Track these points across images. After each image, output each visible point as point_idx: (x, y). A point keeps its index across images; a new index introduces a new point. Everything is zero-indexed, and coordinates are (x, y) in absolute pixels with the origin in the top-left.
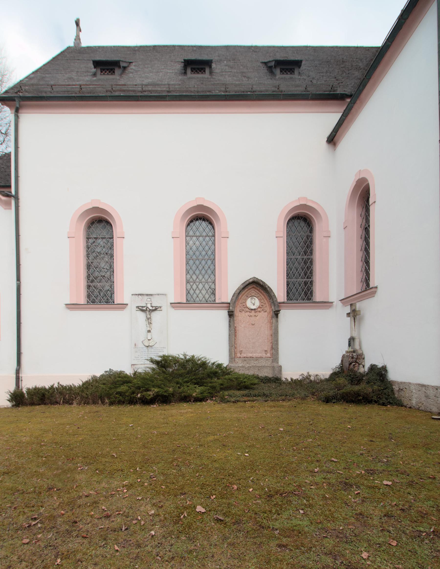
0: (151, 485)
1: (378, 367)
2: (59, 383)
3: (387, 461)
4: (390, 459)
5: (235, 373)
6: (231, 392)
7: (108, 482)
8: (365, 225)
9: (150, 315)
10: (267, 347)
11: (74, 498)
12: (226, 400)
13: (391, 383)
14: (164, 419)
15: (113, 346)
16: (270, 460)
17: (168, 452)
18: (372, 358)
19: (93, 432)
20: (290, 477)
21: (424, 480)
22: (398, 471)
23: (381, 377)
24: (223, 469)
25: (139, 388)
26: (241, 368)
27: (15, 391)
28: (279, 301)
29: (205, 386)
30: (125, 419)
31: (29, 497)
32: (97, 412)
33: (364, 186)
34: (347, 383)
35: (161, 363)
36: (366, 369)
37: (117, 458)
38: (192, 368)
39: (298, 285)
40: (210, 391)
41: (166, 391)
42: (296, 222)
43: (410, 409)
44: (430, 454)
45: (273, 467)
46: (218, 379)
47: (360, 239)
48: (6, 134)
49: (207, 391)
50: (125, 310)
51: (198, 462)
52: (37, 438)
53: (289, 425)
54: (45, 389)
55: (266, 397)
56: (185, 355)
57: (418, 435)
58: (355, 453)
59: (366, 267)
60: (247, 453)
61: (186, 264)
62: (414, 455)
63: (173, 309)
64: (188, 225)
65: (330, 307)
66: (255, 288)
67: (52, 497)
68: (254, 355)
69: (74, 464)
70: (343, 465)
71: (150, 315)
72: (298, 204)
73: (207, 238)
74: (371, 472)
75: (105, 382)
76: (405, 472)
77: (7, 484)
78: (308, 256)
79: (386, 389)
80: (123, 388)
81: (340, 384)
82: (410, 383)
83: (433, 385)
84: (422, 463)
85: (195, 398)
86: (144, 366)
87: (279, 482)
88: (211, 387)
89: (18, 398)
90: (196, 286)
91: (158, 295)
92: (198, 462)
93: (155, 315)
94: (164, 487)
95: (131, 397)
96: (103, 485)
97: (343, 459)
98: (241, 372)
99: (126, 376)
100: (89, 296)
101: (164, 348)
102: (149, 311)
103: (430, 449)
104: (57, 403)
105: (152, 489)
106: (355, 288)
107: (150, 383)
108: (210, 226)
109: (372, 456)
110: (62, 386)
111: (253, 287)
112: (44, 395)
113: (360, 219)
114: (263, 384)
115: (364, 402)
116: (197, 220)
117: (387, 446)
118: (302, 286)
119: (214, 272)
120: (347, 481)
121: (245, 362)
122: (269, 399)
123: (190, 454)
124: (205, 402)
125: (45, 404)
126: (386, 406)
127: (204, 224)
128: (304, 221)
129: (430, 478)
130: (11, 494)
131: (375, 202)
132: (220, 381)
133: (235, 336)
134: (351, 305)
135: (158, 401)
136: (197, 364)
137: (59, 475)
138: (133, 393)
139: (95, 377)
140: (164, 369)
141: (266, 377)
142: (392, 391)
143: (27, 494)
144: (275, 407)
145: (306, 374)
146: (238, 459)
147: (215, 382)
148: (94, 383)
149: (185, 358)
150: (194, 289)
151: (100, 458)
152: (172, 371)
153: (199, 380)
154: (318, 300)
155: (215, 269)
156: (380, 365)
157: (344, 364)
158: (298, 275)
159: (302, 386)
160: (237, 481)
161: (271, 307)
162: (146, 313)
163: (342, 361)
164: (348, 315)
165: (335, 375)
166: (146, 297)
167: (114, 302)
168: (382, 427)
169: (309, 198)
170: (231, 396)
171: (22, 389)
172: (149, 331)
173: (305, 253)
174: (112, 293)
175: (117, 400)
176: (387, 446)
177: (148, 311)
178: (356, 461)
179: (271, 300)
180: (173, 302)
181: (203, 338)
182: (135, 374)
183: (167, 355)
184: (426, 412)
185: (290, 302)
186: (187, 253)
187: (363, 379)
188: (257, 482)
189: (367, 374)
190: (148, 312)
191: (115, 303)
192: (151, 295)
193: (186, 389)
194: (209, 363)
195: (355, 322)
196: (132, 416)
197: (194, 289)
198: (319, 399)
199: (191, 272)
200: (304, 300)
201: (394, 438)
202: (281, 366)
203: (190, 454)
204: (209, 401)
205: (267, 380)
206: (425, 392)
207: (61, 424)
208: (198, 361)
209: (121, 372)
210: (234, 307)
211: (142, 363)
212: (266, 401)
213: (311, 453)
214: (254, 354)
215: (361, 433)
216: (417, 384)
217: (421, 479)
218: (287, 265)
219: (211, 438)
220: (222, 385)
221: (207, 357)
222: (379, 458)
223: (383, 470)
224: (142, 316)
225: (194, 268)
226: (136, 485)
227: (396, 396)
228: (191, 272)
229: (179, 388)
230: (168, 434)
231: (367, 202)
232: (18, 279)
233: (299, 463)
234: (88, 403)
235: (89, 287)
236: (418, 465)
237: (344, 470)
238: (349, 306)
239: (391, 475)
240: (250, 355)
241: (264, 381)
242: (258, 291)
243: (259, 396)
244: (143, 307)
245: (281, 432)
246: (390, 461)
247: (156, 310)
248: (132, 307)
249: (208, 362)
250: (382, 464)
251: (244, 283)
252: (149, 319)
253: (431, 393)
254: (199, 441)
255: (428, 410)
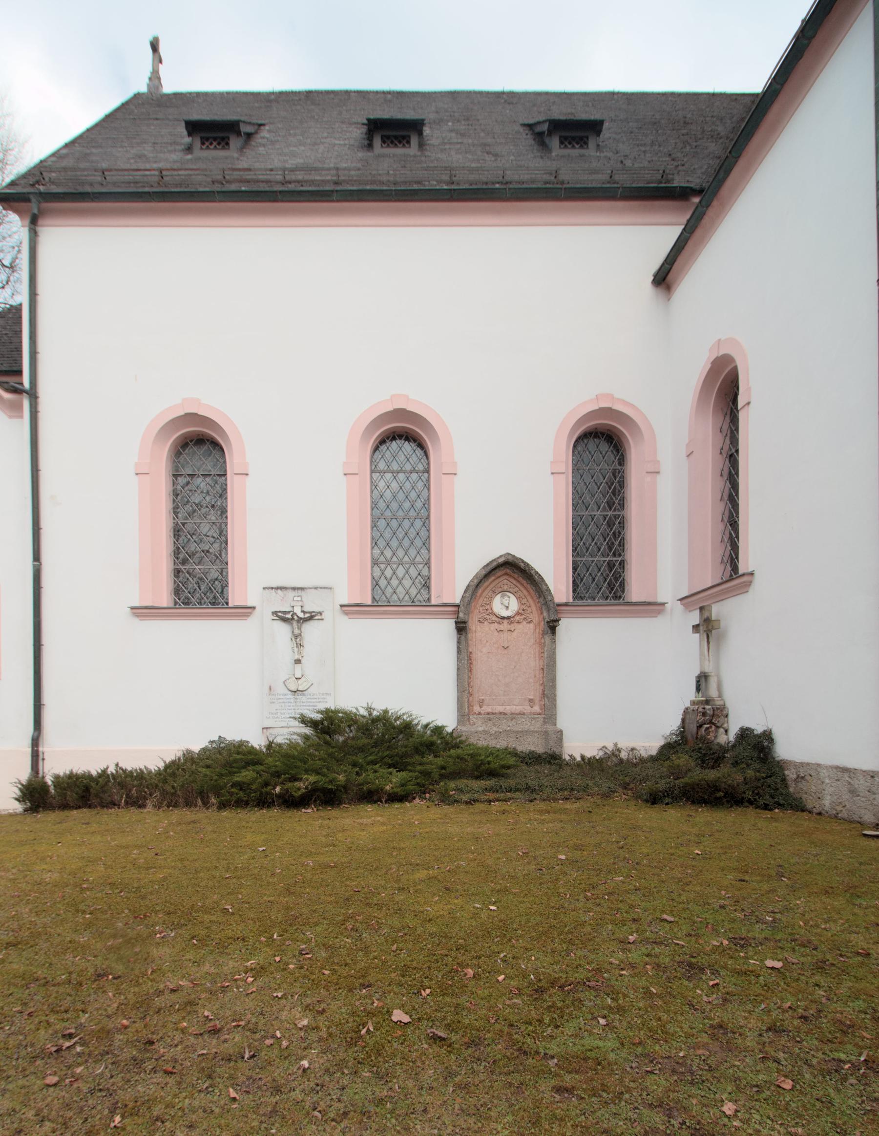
0: (302, 968)
1: (755, 732)
2: (117, 765)
3: (774, 921)
4: (778, 916)
5: (469, 745)
6: (462, 783)
7: (215, 963)
8: (730, 449)
9: (299, 628)
10: (534, 692)
11: (148, 994)
12: (451, 799)
13: (781, 765)
14: (327, 836)
15: (226, 690)
16: (539, 919)
17: (337, 902)
18: (743, 715)
19: (186, 863)
20: (579, 953)
21: (848, 957)
22: (794, 940)
23: (760, 752)
24: (446, 937)
25: (277, 774)
26: (482, 735)
27: (30, 781)
28: (557, 600)
29: (411, 771)
30: (249, 837)
31: (57, 992)
32: (194, 822)
33: (726, 371)
34: (693, 764)
35: (322, 724)
36: (732, 736)
37: (233, 914)
38: (383, 735)
39: (596, 570)
40: (419, 781)
41: (331, 782)
42: (592, 444)
43: (818, 817)
44: (860, 906)
45: (545, 933)
46: (436, 756)
47: (719, 477)
48: (12, 267)
49: (414, 781)
50: (249, 619)
51: (396, 922)
52: (73, 874)
53: (577, 848)
54: (90, 776)
55: (532, 792)
56: (369, 709)
57: (836, 868)
58: (709, 904)
59: (731, 534)
60: (494, 904)
61: (372, 528)
62: (826, 908)
63: (345, 618)
64: (376, 449)
65: (659, 612)
66: (510, 576)
67: (104, 992)
68: (508, 709)
69: (147, 926)
70: (686, 929)
71: (299, 628)
72: (595, 407)
73: (414, 476)
74: (742, 942)
75: (209, 762)
76: (809, 941)
77: (15, 966)
78: (615, 510)
79: (771, 777)
80: (247, 775)
81: (678, 766)
82: (819, 765)
83: (865, 768)
84: (843, 924)
85: (389, 795)
86: (287, 730)
87: (557, 963)
88: (421, 772)
89: (36, 796)
90: (391, 572)
91: (316, 588)
92: (396, 922)
93: (309, 629)
94: (327, 972)
95: (261, 793)
96: (207, 967)
97: (685, 915)
98: (482, 743)
99: (252, 751)
100: (177, 592)
101: (327, 694)
102: (298, 621)
103: (858, 897)
104: (114, 804)
105: (304, 977)
106: (709, 574)
107: (299, 764)
108: (419, 452)
109: (743, 910)
110: (124, 771)
111: (506, 574)
112: (87, 789)
113: (720, 437)
114: (525, 767)
115: (728, 802)
116: (394, 439)
117: (773, 891)
118: (603, 570)
119: (427, 543)
120: (693, 960)
121: (490, 724)
122: (538, 797)
123: (379, 906)
124: (410, 802)
125: (90, 807)
126: (771, 810)
127: (408, 447)
128: (608, 442)
129: (858, 954)
130: (22, 986)
131: (749, 403)
132: (440, 761)
133: (470, 671)
134: (702, 609)
135: (315, 801)
136: (394, 728)
137: (119, 949)
138: (266, 784)
139: (189, 752)
140: (328, 738)
141: (532, 752)
142: (784, 780)
143: (54, 985)
144: (549, 812)
145: (610, 747)
146: (475, 916)
147: (430, 763)
148: (189, 764)
149: (370, 714)
150: (389, 576)
151: (200, 914)
152: (344, 742)
153: (397, 758)
154: (634, 599)
155: (429, 537)
156: (759, 729)
157: (686, 726)
158: (596, 550)
159: (603, 770)
160: (474, 961)
161: (542, 613)
162: (292, 624)
163: (683, 720)
164: (696, 628)
165: (668, 749)
166: (291, 594)
167: (227, 604)
168: (764, 853)
169: (617, 396)
170: (462, 791)
171: (43, 777)
172: (298, 661)
173: (610, 505)
174: (225, 586)
175: (234, 799)
176: (773, 891)
177: (295, 620)
178: (711, 921)
179: (541, 599)
180: (345, 602)
181: (405, 675)
182: (270, 746)
183: (333, 708)
184: (851, 822)
185: (580, 602)
186: (374, 505)
187: (724, 757)
188: (514, 962)
189: (734, 746)
190: (295, 624)
191: (230, 605)
192: (302, 589)
193: (372, 776)
194: (417, 724)
195: (708, 642)
196: (263, 830)
197: (389, 576)
198: (637, 797)
199: (382, 543)
200: (607, 598)
201: (786, 875)
202: (561, 732)
203: (379, 906)
204: (417, 800)
205: (533, 759)
206: (849, 783)
207: (122, 847)
208: (396, 720)
209: (242, 743)
210: (468, 613)
211: (285, 724)
212: (531, 801)
213: (620, 905)
214: (508, 708)
215: (722, 864)
216: (832, 767)
217: (841, 956)
218: (574, 528)
219: (422, 874)
220: (443, 768)
221: (414, 713)
222: (757, 913)
223: (766, 939)
224: (283, 631)
225: (387, 534)
226: (272, 969)
227: (791, 790)
228: (382, 543)
229: (358, 774)
230: (335, 866)
231: (733, 404)
232: (37, 557)
233: (598, 925)
234: (176, 806)
235: (177, 572)
236: (835, 928)
237: (688, 939)
238: (698, 611)
239: (782, 948)
240: (500, 709)
241: (527, 760)
242: (515, 582)
243: (518, 790)
244: (285, 613)
245: (562, 863)
246: (780, 920)
247: (311, 618)
248: (264, 613)
249: (415, 722)
250: (764, 927)
251: (488, 565)
252: (297, 637)
253: (861, 784)
254: (398, 881)
255: (856, 818)
